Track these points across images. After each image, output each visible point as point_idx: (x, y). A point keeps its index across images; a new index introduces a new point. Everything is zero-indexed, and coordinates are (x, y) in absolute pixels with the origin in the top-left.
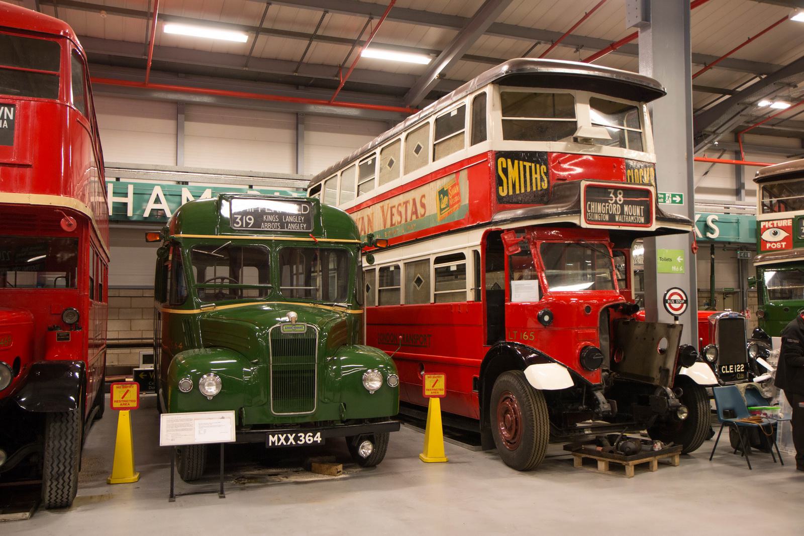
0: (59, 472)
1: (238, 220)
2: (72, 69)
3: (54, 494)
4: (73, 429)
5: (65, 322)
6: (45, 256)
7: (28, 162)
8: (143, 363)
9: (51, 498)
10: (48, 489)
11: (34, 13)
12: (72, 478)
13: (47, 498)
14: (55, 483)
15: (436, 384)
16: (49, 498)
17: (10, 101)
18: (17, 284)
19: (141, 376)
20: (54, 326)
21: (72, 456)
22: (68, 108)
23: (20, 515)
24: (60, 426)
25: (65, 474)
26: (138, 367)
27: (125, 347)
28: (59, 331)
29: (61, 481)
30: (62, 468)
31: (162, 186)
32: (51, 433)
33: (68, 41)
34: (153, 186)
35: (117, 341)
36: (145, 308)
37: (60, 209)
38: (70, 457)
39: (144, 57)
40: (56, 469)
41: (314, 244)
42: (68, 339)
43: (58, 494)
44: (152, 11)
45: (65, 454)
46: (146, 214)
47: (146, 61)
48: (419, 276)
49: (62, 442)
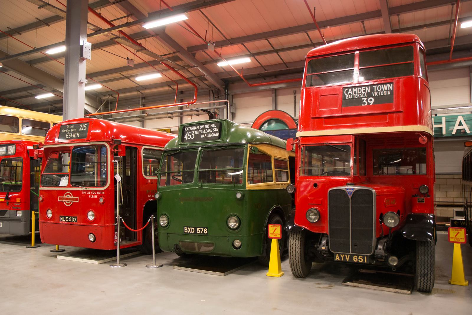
0: (425, 273)
1: (364, 101)
2: (420, 57)
3: (422, 285)
4: (431, 251)
5: (421, 193)
6: (400, 160)
7: (401, 110)
8: (456, 216)
9: (421, 286)
10: (419, 281)
11: (399, 35)
12: (432, 277)
13: (419, 286)
14: (423, 279)
15: (275, 231)
16: (419, 286)
17: (390, 81)
18: (389, 173)
19: (455, 223)
20: (415, 195)
21: (432, 266)
22: (419, 78)
23: (405, 291)
24: (424, 249)
25: (428, 275)
26: (453, 218)
27: (455, 207)
28: (418, 197)
29: (426, 278)
30: (426, 272)
31: (463, 116)
32: (419, 252)
33: (417, 43)
34: (457, 116)
35: (439, 203)
36: (455, 185)
37: (418, 132)
38: (430, 266)
39: (448, 46)
40: (423, 271)
42: (424, 202)
43: (424, 285)
44: (454, 18)
45: (428, 264)
46: (454, 133)
47: (450, 48)
49: (426, 257)
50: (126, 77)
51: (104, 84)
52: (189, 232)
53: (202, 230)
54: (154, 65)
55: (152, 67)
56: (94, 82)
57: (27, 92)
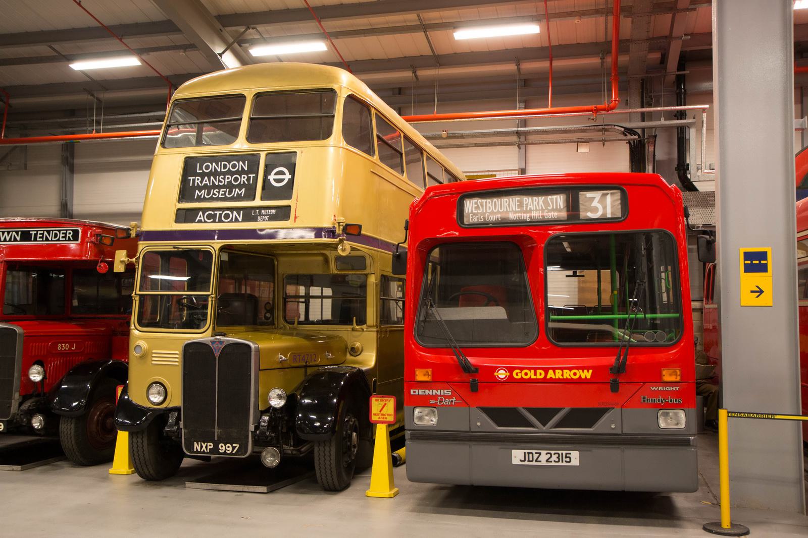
41: (209, 217)
48: (80, 231)
50: (63, 56)
51: (145, 57)
52: (204, 450)
53: (236, 447)
54: (122, 36)
55: (118, 41)
56: (125, 48)
57: (50, 47)
